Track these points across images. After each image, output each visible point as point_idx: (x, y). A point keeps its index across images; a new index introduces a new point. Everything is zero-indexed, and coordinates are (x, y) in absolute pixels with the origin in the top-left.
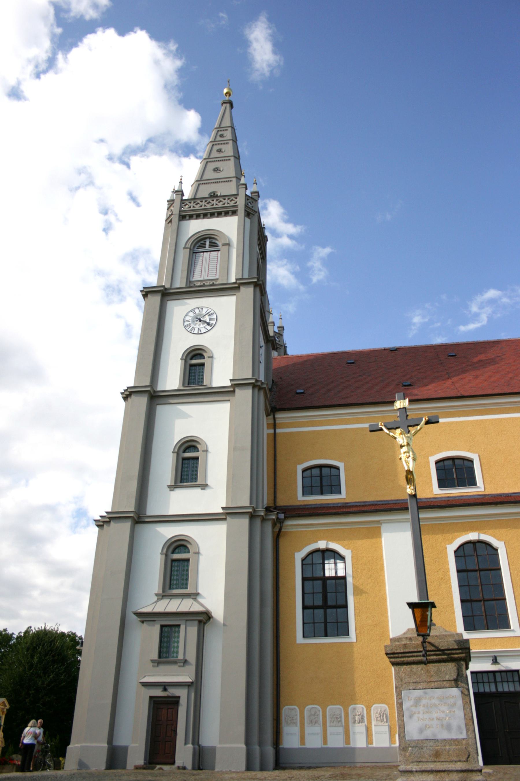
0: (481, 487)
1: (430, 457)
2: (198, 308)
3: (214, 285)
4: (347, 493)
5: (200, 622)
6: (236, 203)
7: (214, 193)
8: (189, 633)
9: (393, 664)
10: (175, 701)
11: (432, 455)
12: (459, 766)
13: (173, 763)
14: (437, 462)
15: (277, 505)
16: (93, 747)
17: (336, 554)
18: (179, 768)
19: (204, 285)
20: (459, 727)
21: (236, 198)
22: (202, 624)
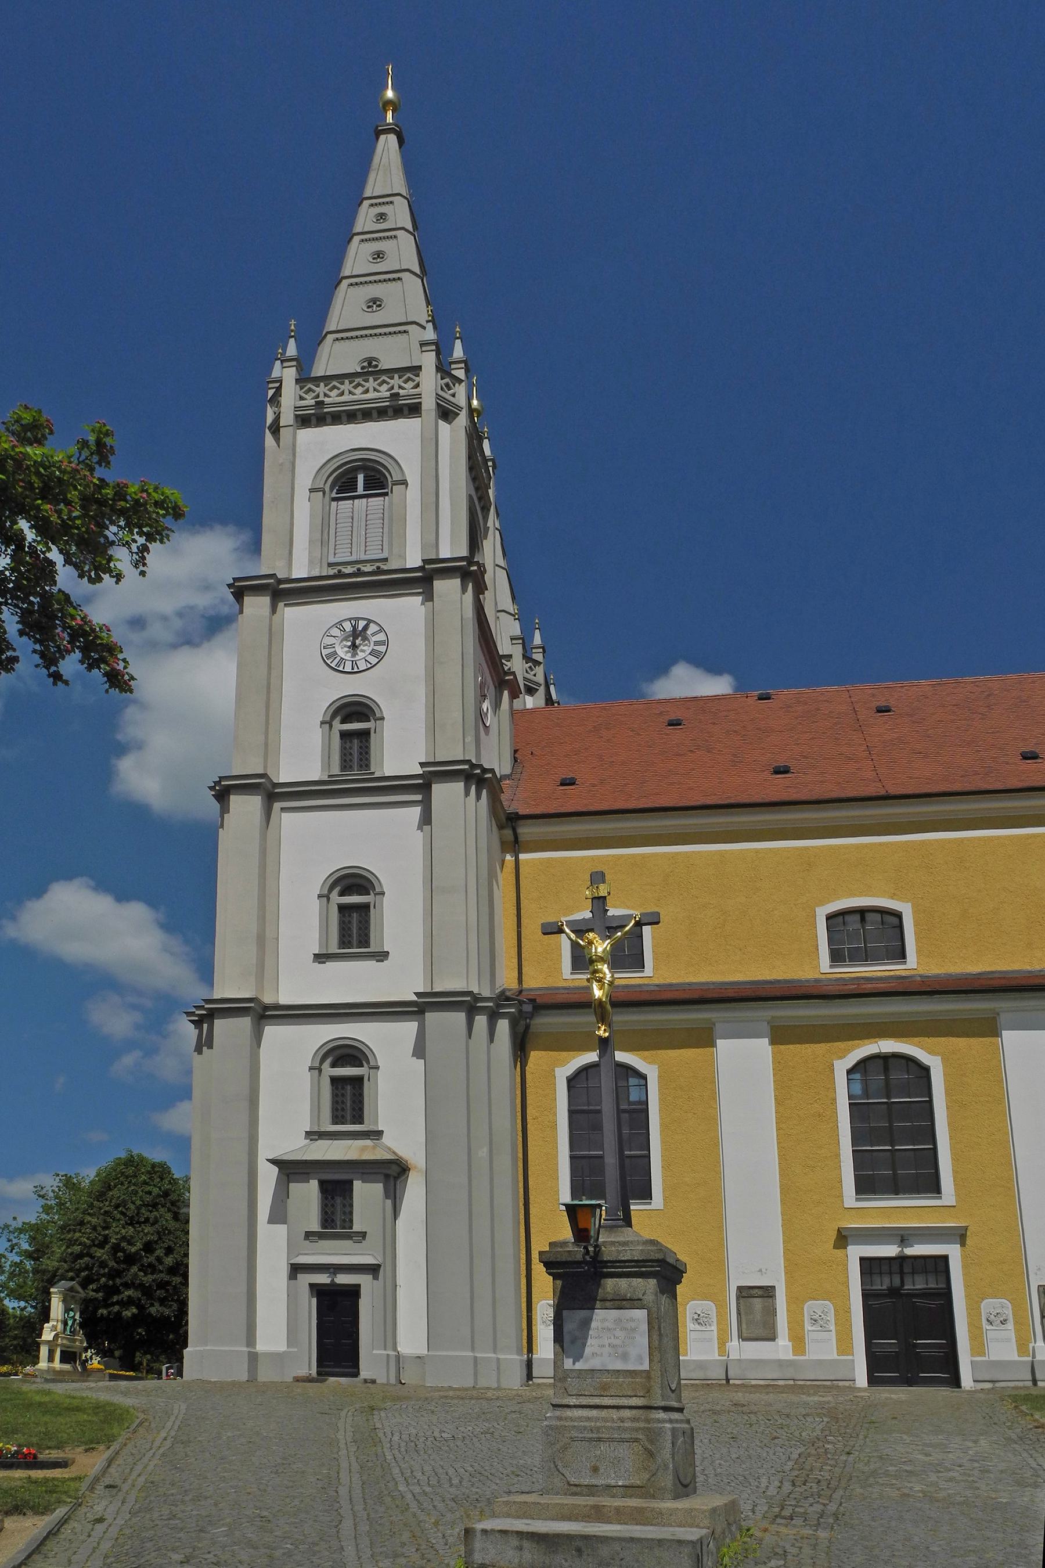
0: (914, 963)
1: (477, 1017)
3: (379, 571)
4: (655, 968)
5: (387, 1176)
6: (417, 386)
7: (370, 361)
8: (366, 1194)
9: (550, 1274)
10: (353, 1292)
11: (822, 903)
12: (639, 1402)
13: (356, 1374)
15: (525, 986)
16: (225, 1351)
18: (366, 1381)
19: (359, 573)
20: (640, 1358)
21: (418, 376)
22: (392, 1179)
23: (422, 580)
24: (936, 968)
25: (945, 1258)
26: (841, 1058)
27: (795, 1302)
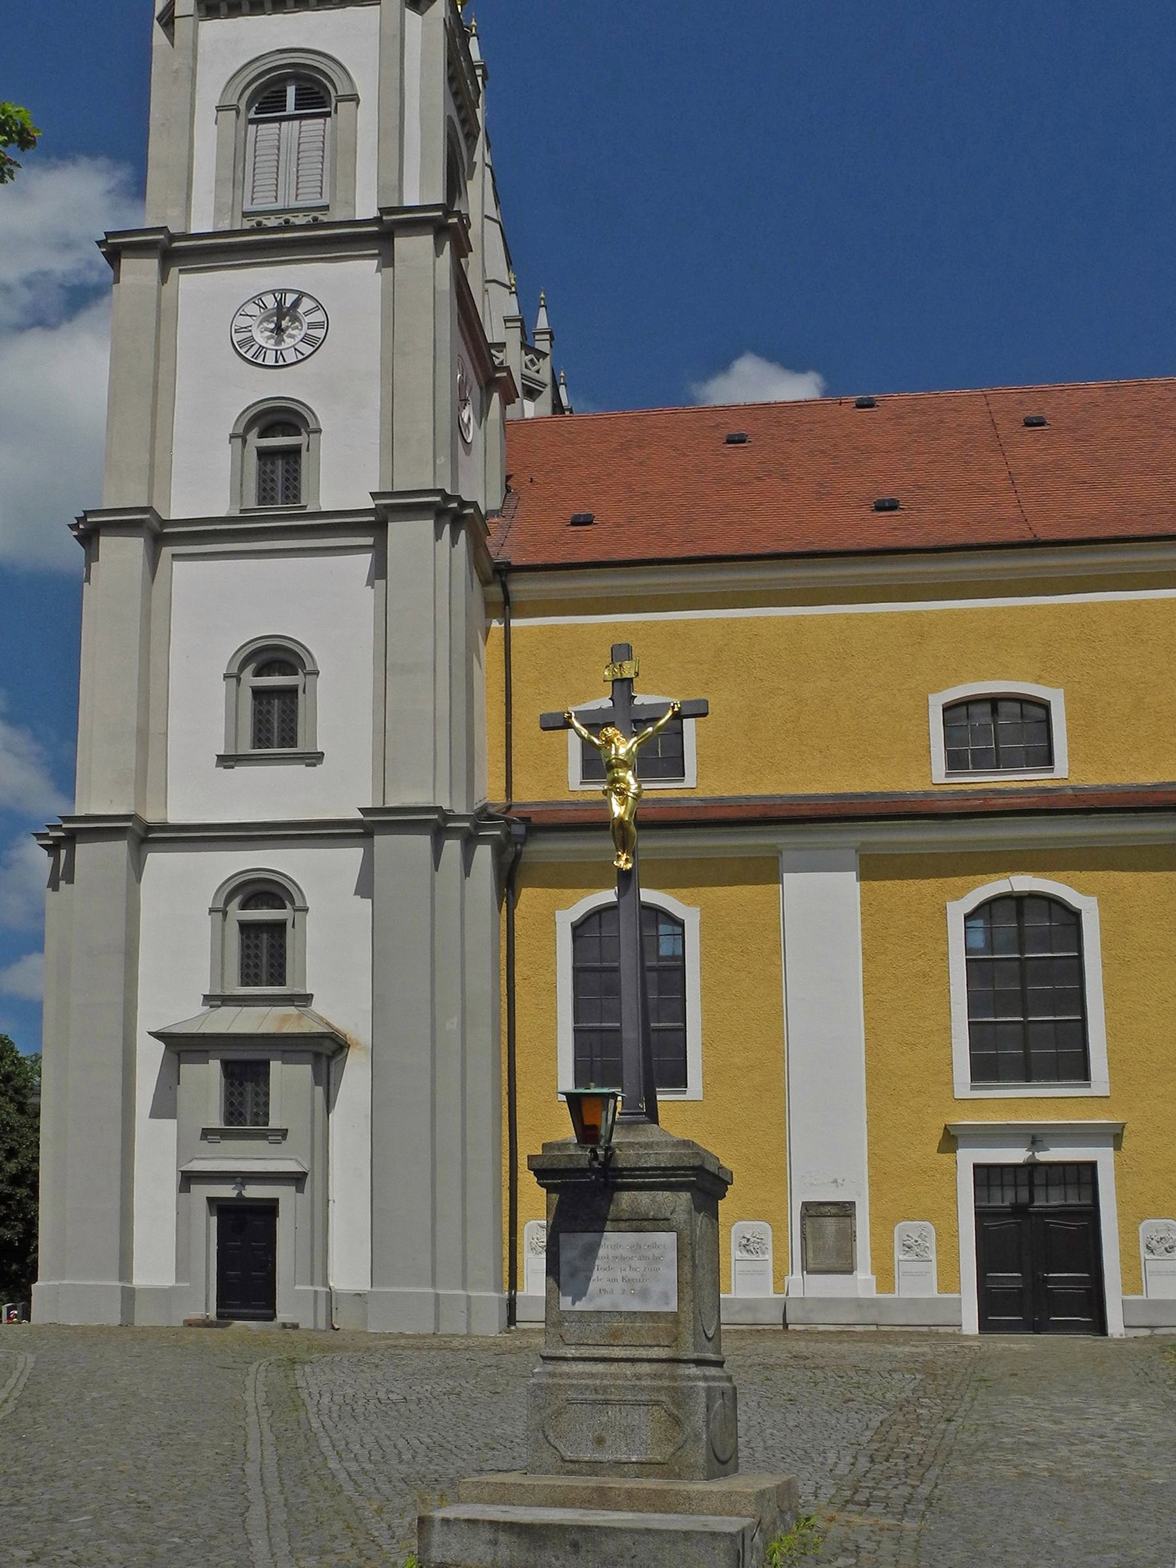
0: (1063, 771)
2: (273, 292)
3: (316, 224)
5: (317, 1055)
8: (288, 1080)
11: (937, 689)
13: (272, 1317)
14: (947, 708)
17: (1053, 905)
18: (284, 1326)
19: (287, 226)
22: (324, 1059)
23: (379, 237)
24: (1094, 778)
25: (1093, 1165)
26: (957, 898)
27: (883, 1223)
